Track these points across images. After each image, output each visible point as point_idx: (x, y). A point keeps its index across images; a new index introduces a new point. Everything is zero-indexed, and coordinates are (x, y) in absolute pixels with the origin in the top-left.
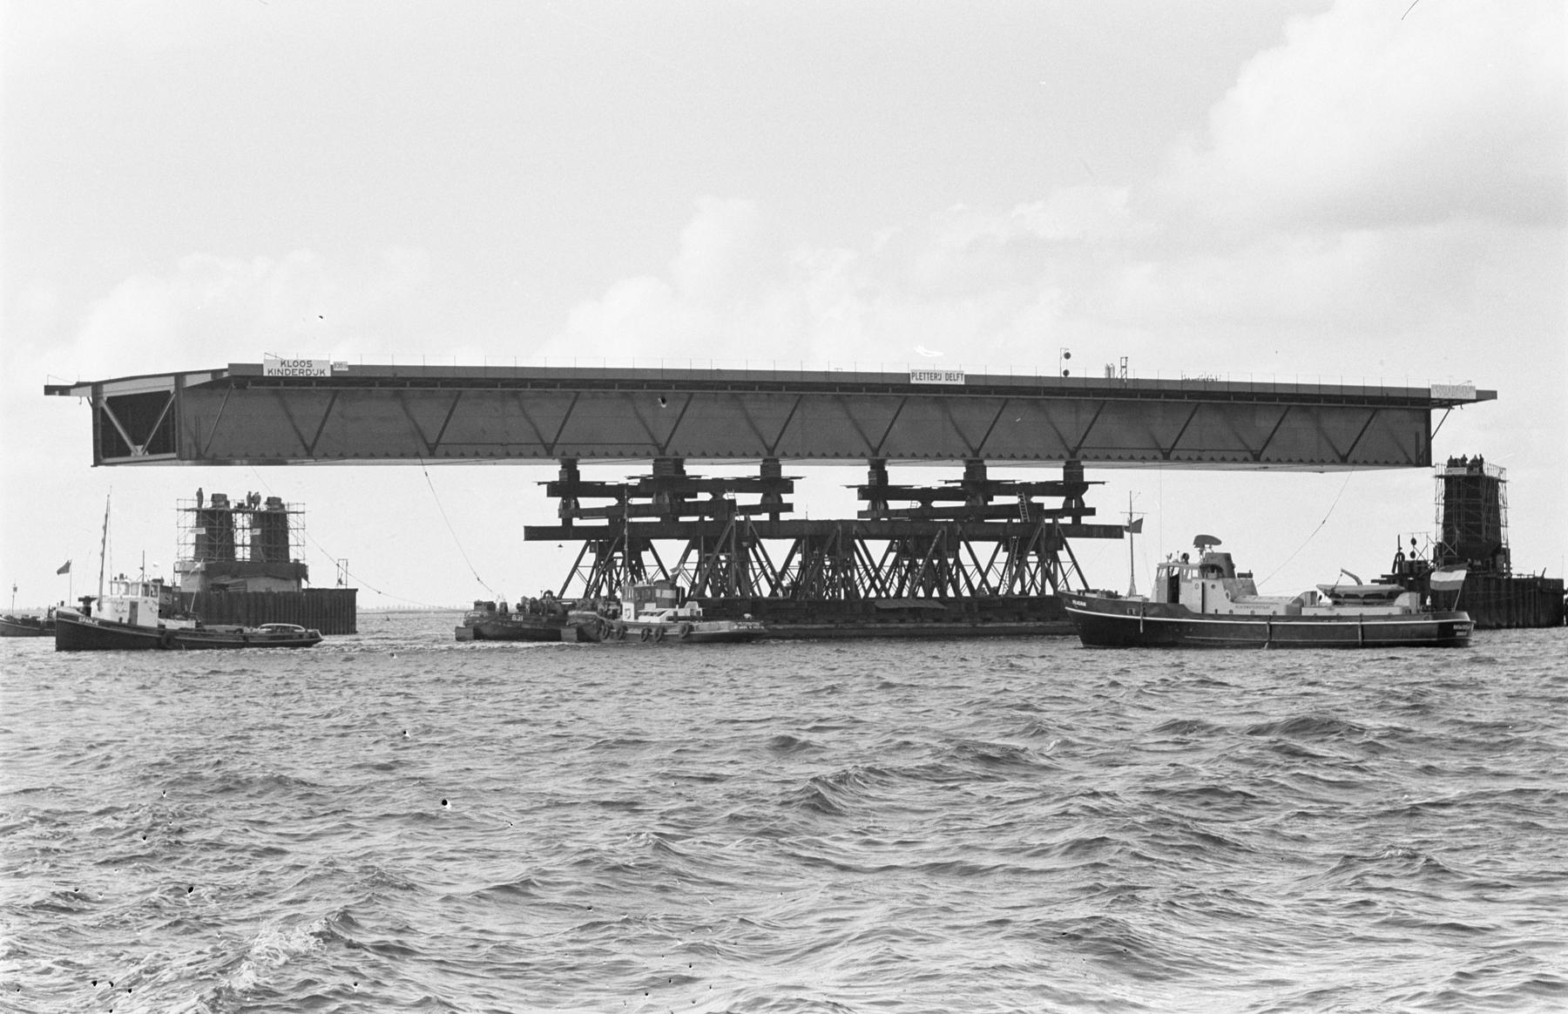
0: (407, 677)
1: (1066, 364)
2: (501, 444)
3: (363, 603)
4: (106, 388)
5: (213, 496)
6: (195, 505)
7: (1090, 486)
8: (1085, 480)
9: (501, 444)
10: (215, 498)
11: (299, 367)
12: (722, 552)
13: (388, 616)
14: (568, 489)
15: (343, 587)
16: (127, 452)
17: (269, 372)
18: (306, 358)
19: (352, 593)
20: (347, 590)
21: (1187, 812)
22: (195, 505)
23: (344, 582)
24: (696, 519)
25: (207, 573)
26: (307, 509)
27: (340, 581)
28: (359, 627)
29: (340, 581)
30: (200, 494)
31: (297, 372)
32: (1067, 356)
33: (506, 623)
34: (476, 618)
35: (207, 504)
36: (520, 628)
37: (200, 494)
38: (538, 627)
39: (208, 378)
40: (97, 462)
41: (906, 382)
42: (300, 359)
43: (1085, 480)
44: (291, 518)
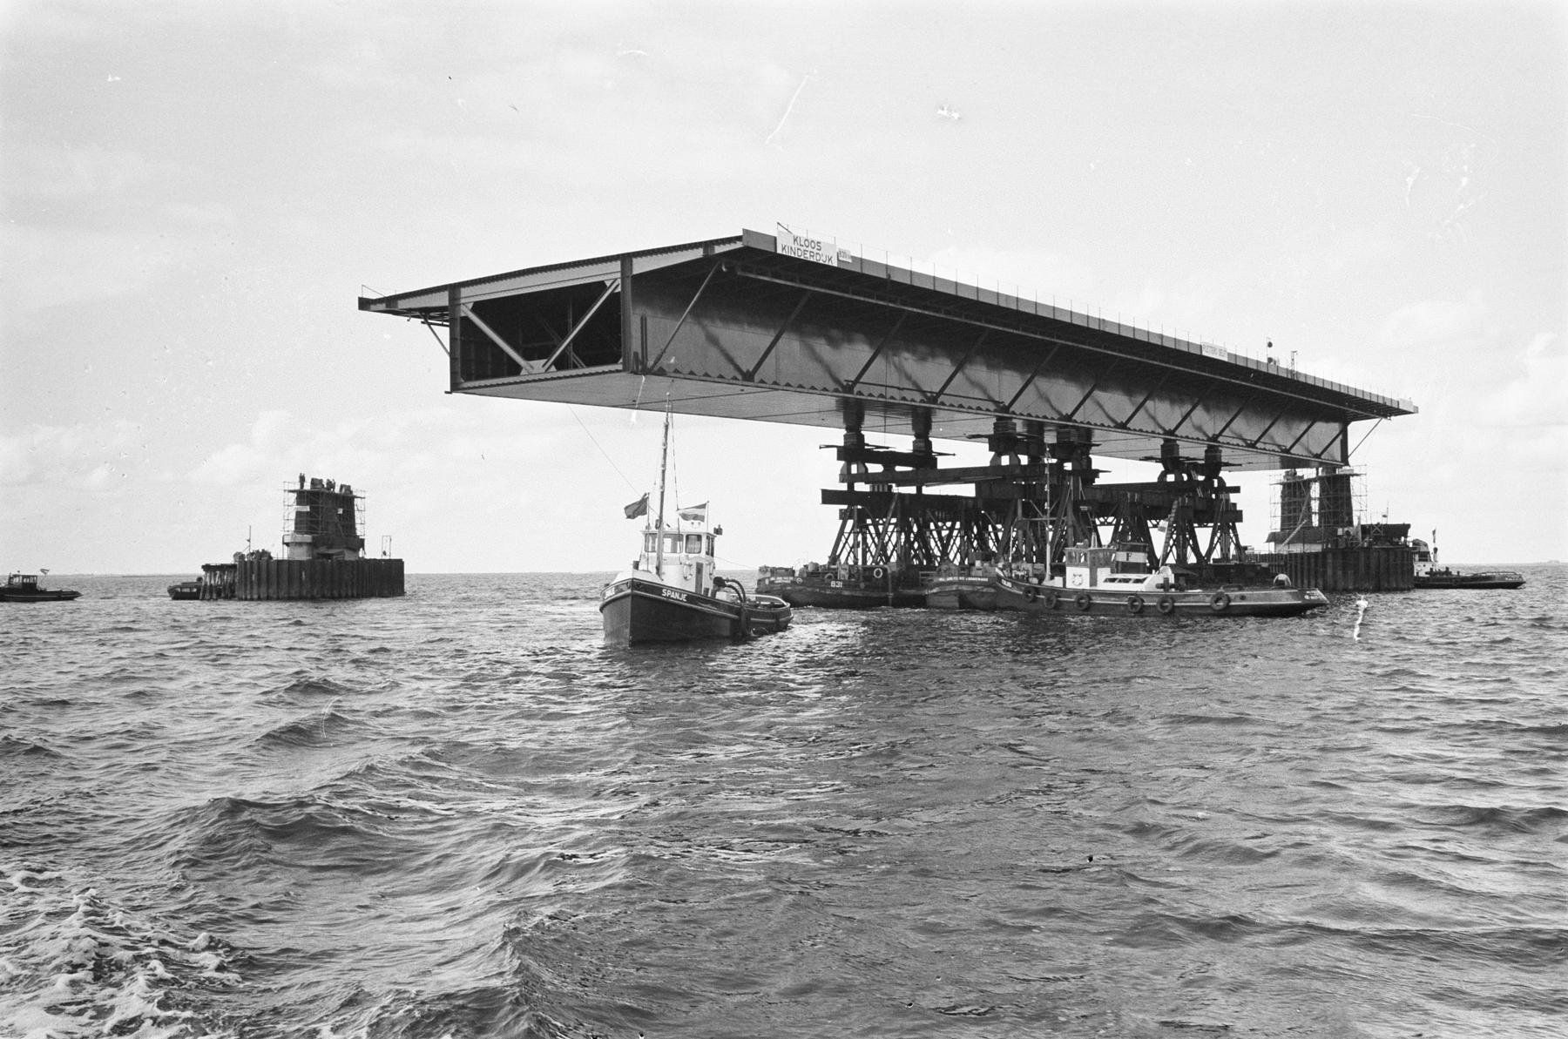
0: (1354, 722)
1: (1272, 353)
2: (899, 388)
3: (408, 570)
4: (464, 292)
5: (313, 480)
6: (297, 487)
7: (1101, 474)
8: (1093, 467)
9: (899, 388)
10: (314, 482)
11: (810, 249)
12: (892, 517)
13: (418, 576)
14: (853, 451)
15: (387, 558)
16: (515, 369)
17: (783, 249)
18: (816, 239)
19: (399, 564)
20: (390, 560)
21: (1474, 755)
22: (297, 487)
23: (388, 553)
24: (926, 490)
25: (313, 545)
26: (367, 495)
27: (385, 553)
28: (407, 587)
29: (385, 553)
30: (302, 479)
31: (808, 255)
32: (1270, 345)
33: (824, 589)
34: (786, 585)
35: (307, 486)
36: (839, 595)
37: (302, 479)
38: (858, 594)
39: (698, 254)
40: (455, 387)
41: (1199, 353)
42: (811, 237)
43: (1093, 467)
44: (357, 501)
